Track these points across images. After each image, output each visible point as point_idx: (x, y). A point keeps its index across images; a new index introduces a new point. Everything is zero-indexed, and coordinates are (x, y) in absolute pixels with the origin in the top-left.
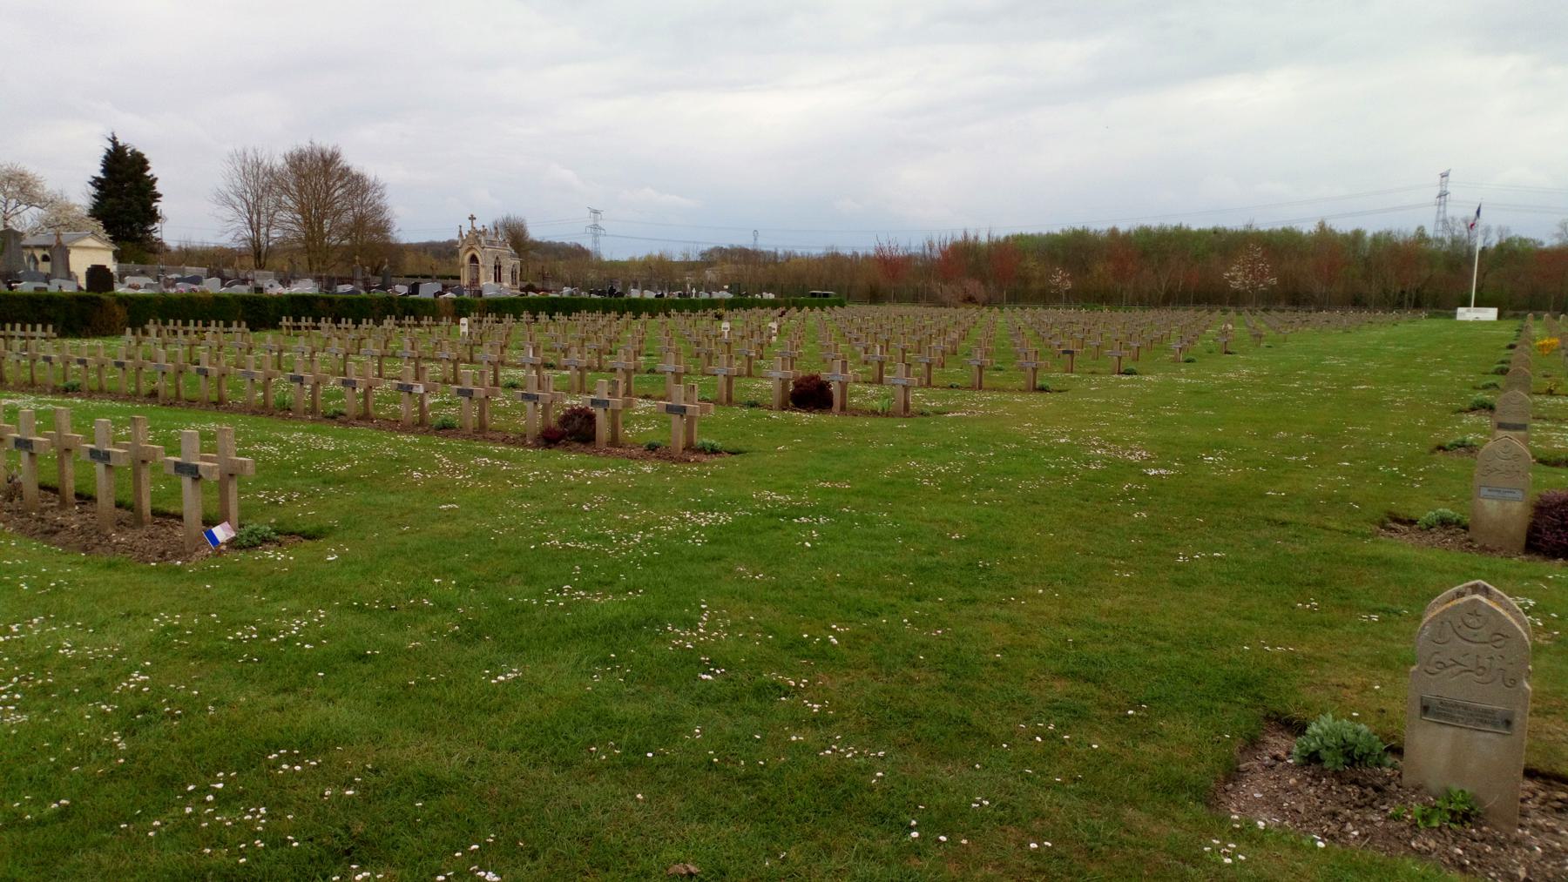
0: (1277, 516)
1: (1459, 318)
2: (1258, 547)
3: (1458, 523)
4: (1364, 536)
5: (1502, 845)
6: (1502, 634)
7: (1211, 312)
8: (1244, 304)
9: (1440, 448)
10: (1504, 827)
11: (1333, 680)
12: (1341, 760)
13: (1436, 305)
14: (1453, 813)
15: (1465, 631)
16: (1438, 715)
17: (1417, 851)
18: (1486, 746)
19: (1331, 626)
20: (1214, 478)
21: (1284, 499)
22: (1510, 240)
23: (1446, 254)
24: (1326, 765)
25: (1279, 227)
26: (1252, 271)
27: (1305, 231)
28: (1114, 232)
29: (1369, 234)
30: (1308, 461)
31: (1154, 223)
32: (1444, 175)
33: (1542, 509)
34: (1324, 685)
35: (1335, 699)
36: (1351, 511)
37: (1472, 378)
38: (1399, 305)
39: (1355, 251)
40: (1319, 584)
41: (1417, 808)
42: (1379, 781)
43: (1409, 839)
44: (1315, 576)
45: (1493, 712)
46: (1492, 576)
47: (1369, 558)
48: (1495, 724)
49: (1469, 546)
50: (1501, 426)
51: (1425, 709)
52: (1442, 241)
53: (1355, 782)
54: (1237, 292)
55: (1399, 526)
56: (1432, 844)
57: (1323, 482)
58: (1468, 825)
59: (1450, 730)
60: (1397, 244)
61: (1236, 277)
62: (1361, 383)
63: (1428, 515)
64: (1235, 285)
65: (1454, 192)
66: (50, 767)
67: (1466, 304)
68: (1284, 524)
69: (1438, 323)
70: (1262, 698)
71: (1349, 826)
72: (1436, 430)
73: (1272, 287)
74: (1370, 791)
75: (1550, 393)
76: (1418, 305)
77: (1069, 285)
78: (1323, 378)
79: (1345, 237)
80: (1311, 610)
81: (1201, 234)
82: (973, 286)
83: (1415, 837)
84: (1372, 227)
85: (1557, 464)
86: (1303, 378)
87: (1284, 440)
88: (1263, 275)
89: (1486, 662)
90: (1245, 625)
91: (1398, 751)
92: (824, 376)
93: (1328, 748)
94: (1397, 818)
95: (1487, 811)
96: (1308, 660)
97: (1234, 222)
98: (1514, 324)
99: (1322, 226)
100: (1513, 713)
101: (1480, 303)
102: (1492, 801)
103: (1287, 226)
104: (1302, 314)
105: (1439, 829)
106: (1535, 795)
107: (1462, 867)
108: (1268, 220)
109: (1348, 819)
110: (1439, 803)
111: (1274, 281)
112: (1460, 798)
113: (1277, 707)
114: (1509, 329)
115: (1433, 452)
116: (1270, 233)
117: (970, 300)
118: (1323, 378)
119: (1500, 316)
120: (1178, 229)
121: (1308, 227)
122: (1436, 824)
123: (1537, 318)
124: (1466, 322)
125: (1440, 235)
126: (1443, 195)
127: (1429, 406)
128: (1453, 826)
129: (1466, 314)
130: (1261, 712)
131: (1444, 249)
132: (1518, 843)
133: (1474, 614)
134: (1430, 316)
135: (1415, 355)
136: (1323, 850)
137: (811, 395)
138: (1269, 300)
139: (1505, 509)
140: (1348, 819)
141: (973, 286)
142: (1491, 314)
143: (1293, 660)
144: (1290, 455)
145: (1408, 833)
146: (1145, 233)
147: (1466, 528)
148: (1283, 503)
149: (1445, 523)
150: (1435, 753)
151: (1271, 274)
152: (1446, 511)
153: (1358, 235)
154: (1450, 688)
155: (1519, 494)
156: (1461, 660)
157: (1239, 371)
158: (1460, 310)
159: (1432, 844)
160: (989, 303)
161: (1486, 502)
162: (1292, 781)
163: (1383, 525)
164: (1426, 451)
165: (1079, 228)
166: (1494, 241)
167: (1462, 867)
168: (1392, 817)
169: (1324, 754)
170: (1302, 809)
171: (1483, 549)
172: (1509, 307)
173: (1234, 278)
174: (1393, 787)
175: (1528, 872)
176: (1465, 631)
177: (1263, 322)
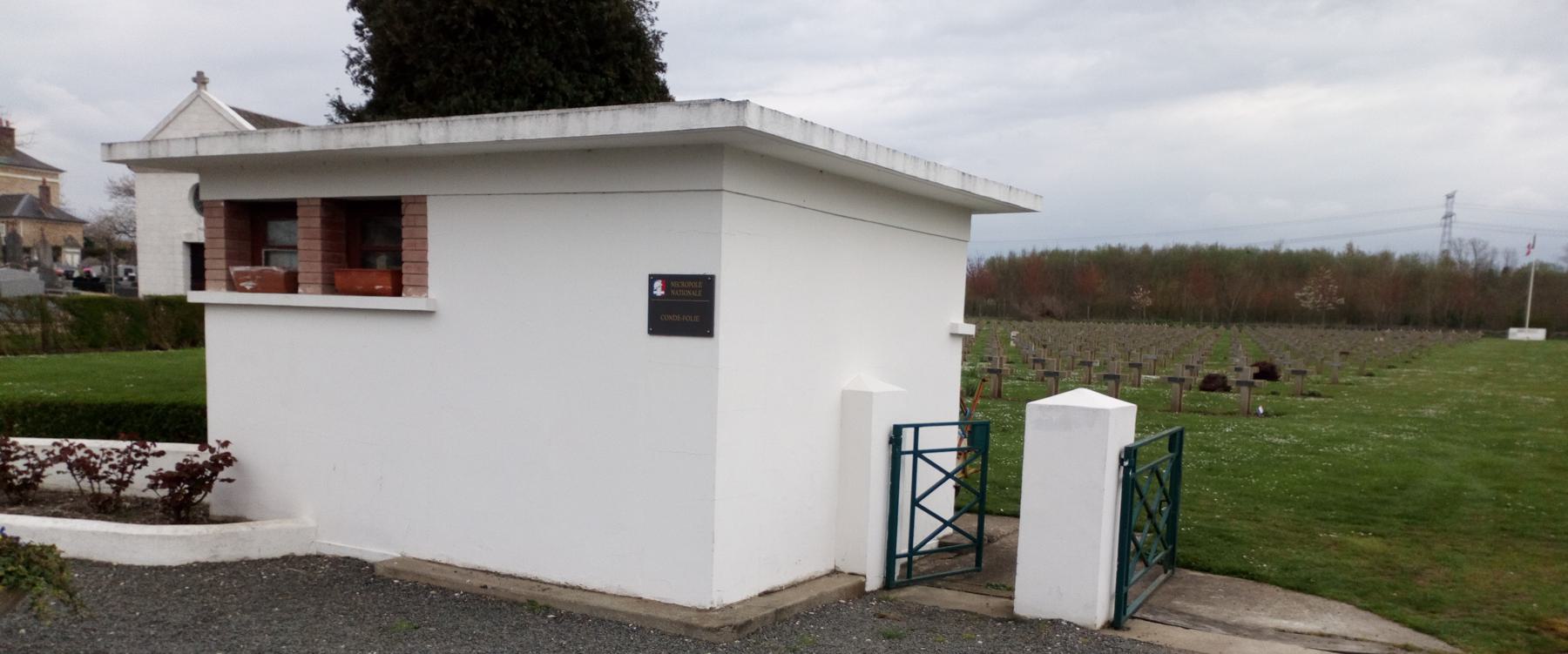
1: (1511, 337)
26: (1322, 291)
28: (1146, 250)
29: (1397, 257)
31: (1190, 241)
32: (1450, 197)
61: (1307, 297)
64: (1308, 304)
65: (1460, 214)
67: (1519, 324)
69: (1498, 342)
73: (1339, 306)
77: (1149, 302)
79: (1373, 259)
81: (1266, 254)
82: (1051, 302)
92: (1277, 361)
99: (1350, 247)
101: (1534, 324)
111: (1342, 301)
117: (1048, 314)
119: (1548, 336)
120: (1213, 249)
121: (1337, 247)
126: (1448, 216)
129: (1515, 334)
137: (1267, 372)
141: (1051, 302)
142: (1539, 334)
146: (1180, 251)
151: (1340, 295)
158: (1512, 331)
160: (1068, 317)
165: (1114, 244)
172: (1558, 327)
173: (1304, 298)
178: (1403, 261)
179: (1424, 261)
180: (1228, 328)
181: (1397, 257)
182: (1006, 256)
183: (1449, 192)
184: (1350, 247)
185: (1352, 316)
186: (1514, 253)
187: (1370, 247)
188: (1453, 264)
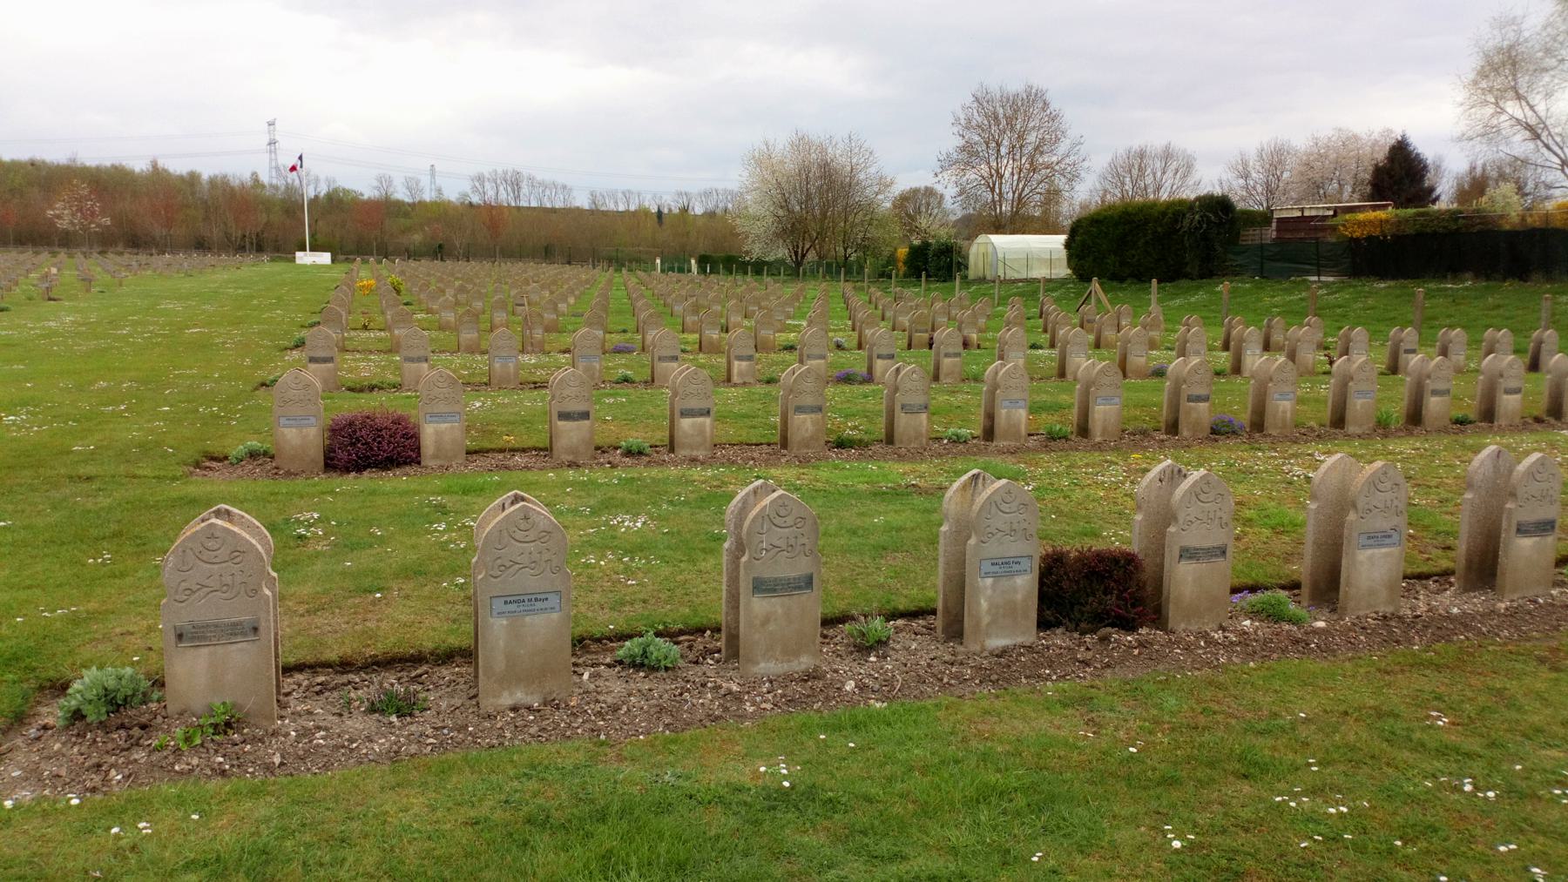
0: (81, 471)
2: (54, 508)
3: (265, 454)
4: (174, 479)
5: (261, 740)
6: (239, 551)
7: (37, 253)
8: (78, 246)
9: (263, 384)
10: (265, 723)
11: (118, 630)
12: (104, 710)
13: (277, 249)
14: (215, 726)
15: (206, 555)
16: (192, 639)
17: (181, 773)
18: (240, 656)
19: (122, 575)
20: (14, 440)
21: (92, 453)
22: (336, 190)
23: (283, 201)
24: (89, 720)
25: (108, 164)
27: (137, 170)
29: (205, 177)
30: (125, 410)
32: (271, 124)
33: (335, 431)
34: (107, 638)
35: (117, 649)
36: (164, 456)
37: (300, 317)
38: (241, 249)
39: (193, 194)
40: (117, 535)
41: (179, 732)
42: (143, 720)
43: (173, 764)
44: (114, 527)
45: (240, 623)
46: (528, 486)
47: (174, 500)
48: (244, 634)
49: (276, 473)
50: (312, 360)
51: (180, 637)
52: (276, 188)
53: (122, 726)
54: (67, 233)
55: (214, 464)
56: (195, 761)
57: (138, 430)
58: (230, 732)
59: (205, 651)
60: (232, 189)
61: (62, 215)
62: (195, 326)
63: (238, 450)
64: (63, 224)
65: (283, 143)
66: (1478, 767)
68: (89, 479)
69: (279, 267)
70: (34, 669)
71: (113, 772)
72: (261, 368)
74: (136, 732)
75: (365, 328)
76: (260, 249)
78: (156, 323)
79: (181, 178)
80: (104, 564)
83: (178, 761)
84: (207, 171)
85: (361, 390)
86: (134, 324)
87: (104, 390)
88: (93, 214)
89: (228, 580)
90: (23, 595)
91: (160, 684)
93: (90, 702)
94: (162, 748)
95: (247, 714)
96: (92, 616)
97: (55, 154)
98: (343, 267)
99: (155, 165)
100: (258, 620)
102: (250, 704)
103: (117, 163)
104: (143, 258)
105: (202, 745)
106: (300, 685)
107: (223, 773)
108: (95, 153)
109: (112, 766)
110: (202, 721)
111: (107, 221)
112: (222, 709)
113: (52, 673)
114: (339, 272)
115: (256, 389)
116: (98, 169)
118: (156, 323)
119: (333, 261)
121: (140, 165)
122: (198, 741)
123: (365, 262)
124: (305, 266)
125: (274, 182)
126: (272, 143)
127: (258, 345)
128: (217, 738)
129: (305, 258)
130: (33, 684)
131: (279, 195)
132: (274, 734)
133: (212, 537)
134: (273, 260)
135: (253, 297)
136: (78, 806)
138: (105, 242)
139: (303, 435)
140: (112, 766)
142: (325, 258)
143: (75, 620)
144: (106, 405)
145: (171, 759)
147: (272, 457)
148: (91, 457)
149: (253, 455)
150: (196, 678)
151: (103, 213)
152: (254, 443)
153: (193, 178)
154: (199, 611)
155: (313, 420)
156: (206, 582)
157: (62, 318)
158: (299, 254)
159: (195, 761)
161: (286, 431)
162: (57, 746)
163: (197, 465)
164: (249, 388)
166: (323, 190)
167: (223, 773)
168: (155, 749)
169: (87, 709)
170: (63, 772)
171: (289, 474)
172: (341, 253)
173: (59, 217)
174: (159, 719)
175: (283, 757)
176: (206, 555)
177: (97, 266)
178: (213, 182)
179: (235, 183)
180: (71, 256)
181: (205, 177)
182: (246, 176)
183: (270, 119)
184: (155, 165)
185: (439, 251)
186: (390, 182)
187: (178, 166)
188: (263, 186)
